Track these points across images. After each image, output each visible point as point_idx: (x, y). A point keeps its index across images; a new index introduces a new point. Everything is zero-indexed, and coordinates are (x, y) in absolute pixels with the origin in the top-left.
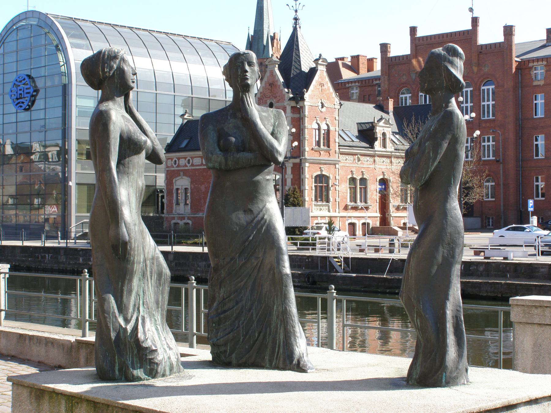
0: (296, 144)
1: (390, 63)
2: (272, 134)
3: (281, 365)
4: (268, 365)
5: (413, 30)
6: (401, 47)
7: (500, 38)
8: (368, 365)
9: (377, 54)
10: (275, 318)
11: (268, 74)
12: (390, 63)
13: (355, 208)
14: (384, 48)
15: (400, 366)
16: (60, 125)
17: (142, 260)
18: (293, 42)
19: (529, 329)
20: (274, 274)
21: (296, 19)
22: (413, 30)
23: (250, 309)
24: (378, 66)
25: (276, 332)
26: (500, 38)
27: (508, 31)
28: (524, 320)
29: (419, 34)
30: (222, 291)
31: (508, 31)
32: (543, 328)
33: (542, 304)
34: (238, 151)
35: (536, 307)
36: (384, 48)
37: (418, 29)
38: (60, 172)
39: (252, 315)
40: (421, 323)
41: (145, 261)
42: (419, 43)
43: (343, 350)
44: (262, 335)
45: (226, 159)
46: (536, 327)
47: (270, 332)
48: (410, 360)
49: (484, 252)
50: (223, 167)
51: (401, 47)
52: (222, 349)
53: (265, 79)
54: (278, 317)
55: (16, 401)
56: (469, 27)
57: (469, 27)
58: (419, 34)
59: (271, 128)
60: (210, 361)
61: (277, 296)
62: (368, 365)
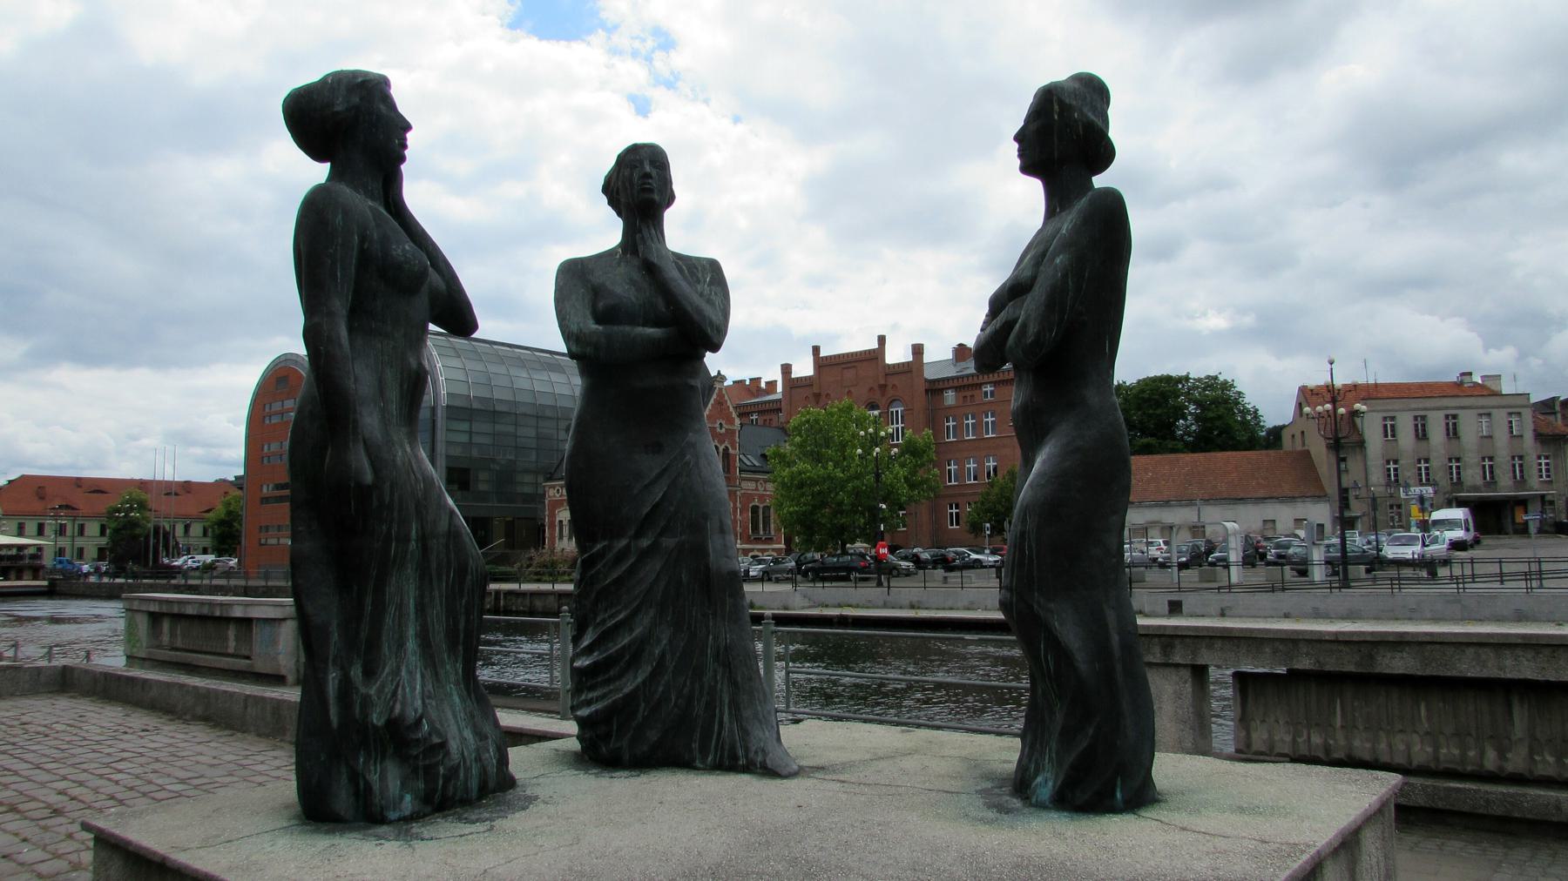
1: (792, 384)
5: (816, 350)
7: (908, 357)
9: (777, 376)
12: (792, 384)
13: (758, 540)
14: (786, 369)
22: (816, 350)
24: (779, 389)
26: (908, 357)
27: (918, 350)
29: (823, 354)
31: (918, 350)
36: (786, 369)
37: (515, 822)
38: (786, 649)
42: (823, 364)
49: (1489, 415)
55: (99, 866)
56: (876, 346)
57: (876, 346)
58: (823, 354)
60: (576, 753)
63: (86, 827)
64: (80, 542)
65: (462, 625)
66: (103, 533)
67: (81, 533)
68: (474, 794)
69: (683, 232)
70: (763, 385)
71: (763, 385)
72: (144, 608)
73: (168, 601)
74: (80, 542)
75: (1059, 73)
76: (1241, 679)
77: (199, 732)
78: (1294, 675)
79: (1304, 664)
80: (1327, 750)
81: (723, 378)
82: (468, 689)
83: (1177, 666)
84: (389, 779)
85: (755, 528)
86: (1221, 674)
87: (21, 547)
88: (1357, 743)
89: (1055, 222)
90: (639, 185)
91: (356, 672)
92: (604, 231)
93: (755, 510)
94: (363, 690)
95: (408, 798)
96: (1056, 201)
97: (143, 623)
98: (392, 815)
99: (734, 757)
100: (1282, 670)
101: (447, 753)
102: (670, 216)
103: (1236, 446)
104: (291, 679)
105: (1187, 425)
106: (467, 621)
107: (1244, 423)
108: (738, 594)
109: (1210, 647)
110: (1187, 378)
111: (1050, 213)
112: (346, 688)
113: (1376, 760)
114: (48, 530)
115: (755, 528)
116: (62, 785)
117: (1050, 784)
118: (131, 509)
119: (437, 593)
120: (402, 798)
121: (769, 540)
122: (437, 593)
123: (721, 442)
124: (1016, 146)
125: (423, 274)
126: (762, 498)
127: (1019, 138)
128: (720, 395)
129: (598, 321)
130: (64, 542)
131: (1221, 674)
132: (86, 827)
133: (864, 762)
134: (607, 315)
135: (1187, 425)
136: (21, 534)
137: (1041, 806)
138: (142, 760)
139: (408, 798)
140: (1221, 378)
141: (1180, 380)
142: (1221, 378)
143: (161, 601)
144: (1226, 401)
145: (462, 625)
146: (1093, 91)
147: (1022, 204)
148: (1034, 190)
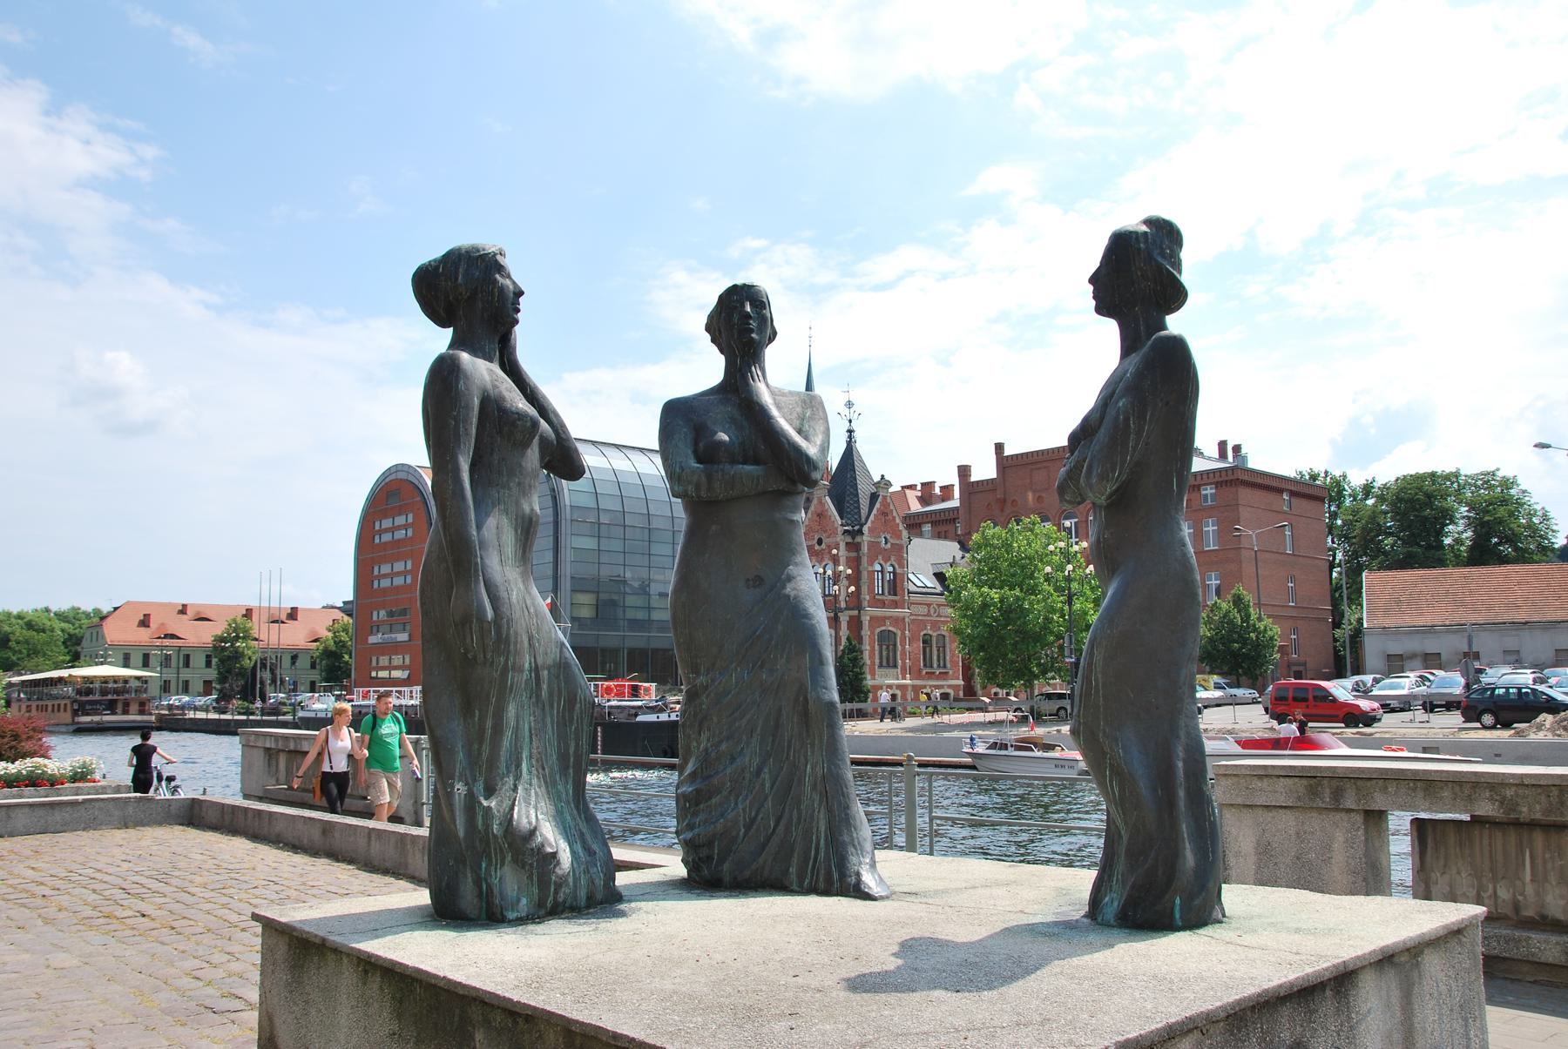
0: (852, 589)
1: (970, 488)
2: (799, 432)
3: (822, 885)
4: (795, 887)
5: (999, 448)
6: (985, 470)
8: (998, 884)
9: (953, 479)
10: (808, 788)
11: (815, 502)
12: (970, 488)
13: (930, 675)
14: (964, 471)
15: (1061, 884)
16: (550, 572)
17: (527, 665)
18: (849, 455)
19: (1247, 816)
20: (806, 699)
21: (850, 431)
22: (999, 448)
23: (759, 772)
24: (957, 494)
25: (812, 817)
28: (1240, 801)
29: (1008, 452)
30: (704, 737)
32: (1274, 813)
33: (1270, 772)
34: (733, 462)
35: (1260, 777)
36: (964, 471)
39: (763, 785)
40: (1122, 790)
41: (536, 669)
43: (931, 854)
44: (783, 822)
45: (709, 477)
46: (1260, 811)
47: (799, 819)
48: (1092, 874)
50: (703, 494)
51: (985, 470)
52: (704, 852)
53: (812, 508)
54: (814, 787)
58: (1008, 452)
59: (798, 423)
61: (813, 745)
62: (998, 884)
63: (255, 917)
64: (186, 674)
65: (572, 750)
66: (208, 664)
67: (187, 664)
68: (583, 903)
69: (779, 373)
70: (937, 491)
71: (937, 491)
72: (259, 744)
73: (286, 738)
74: (186, 674)
75: (1132, 219)
76: (1419, 826)
77: (322, 864)
78: (1476, 820)
79: (1486, 808)
80: (1517, 907)
81: (889, 484)
82: (577, 808)
83: (1349, 811)
84: (509, 882)
85: (928, 663)
86: (1400, 821)
87: (126, 680)
88: (1549, 898)
89: (1128, 360)
90: (740, 323)
91: (479, 787)
92: (704, 369)
93: (927, 641)
94: (485, 803)
95: (524, 901)
96: (1129, 345)
97: (259, 758)
98: (511, 915)
99: (829, 880)
100: (1466, 817)
101: (558, 863)
102: (771, 353)
103: (1522, 557)
104: (407, 819)
105: (1459, 532)
106: (577, 745)
107: (1530, 526)
108: (833, 728)
109: (1384, 790)
110: (1457, 475)
111: (1126, 351)
112: (471, 799)
113: (1544, 917)
114: (152, 661)
115: (928, 663)
116: (208, 906)
117: (1116, 904)
118: (237, 637)
119: (548, 720)
120: (519, 900)
121: (944, 676)
122: (548, 720)
123: (887, 560)
124: (1091, 288)
125: (535, 424)
126: (935, 625)
127: (1093, 280)
128: (885, 504)
129: (699, 462)
130: (170, 675)
131: (1400, 821)
132: (255, 917)
133: (958, 890)
134: (708, 454)
135: (1459, 532)
136: (126, 665)
137: (1106, 925)
138: (277, 888)
139: (524, 901)
140: (1500, 474)
141: (1447, 477)
142: (1500, 474)
143: (276, 737)
144: (1504, 501)
145: (572, 750)
146: (1164, 235)
147: (1099, 349)
148: (1109, 332)
